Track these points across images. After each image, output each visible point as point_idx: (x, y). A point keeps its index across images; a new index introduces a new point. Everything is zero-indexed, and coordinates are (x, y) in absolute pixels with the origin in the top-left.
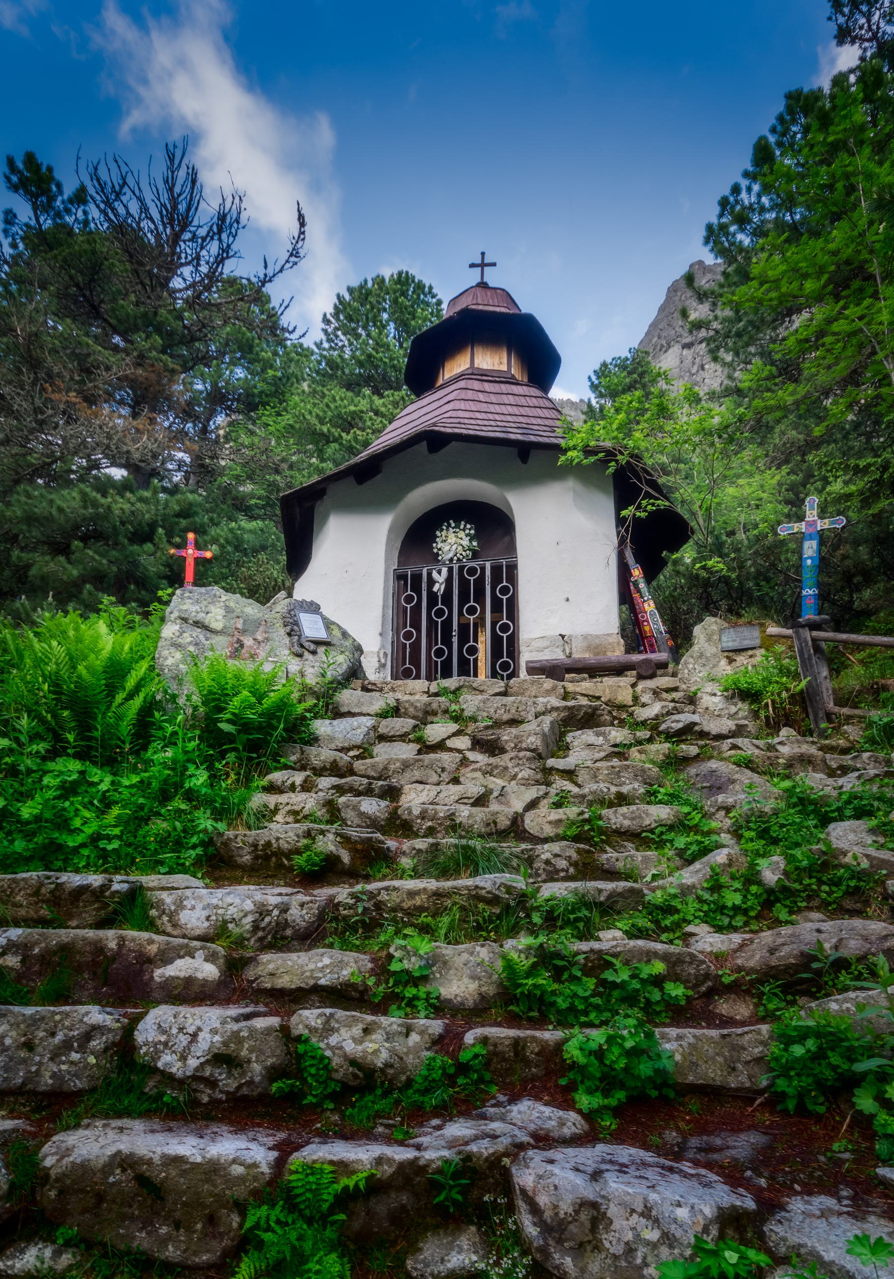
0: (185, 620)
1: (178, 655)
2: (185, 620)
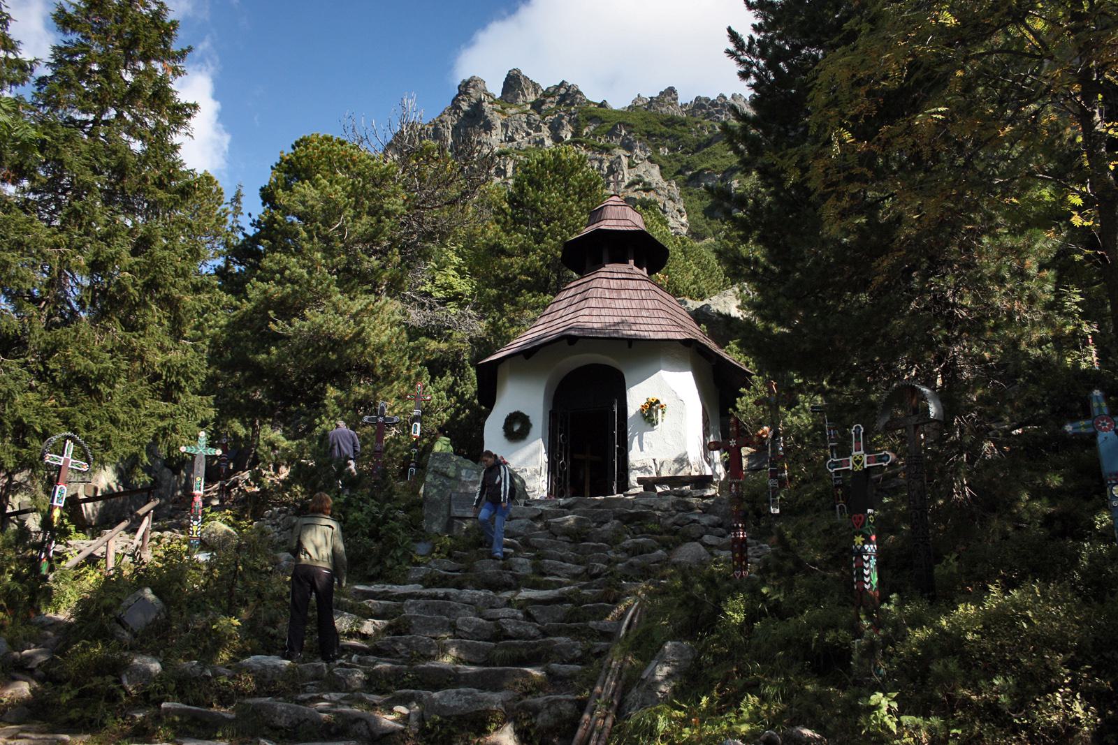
1: (435, 491)
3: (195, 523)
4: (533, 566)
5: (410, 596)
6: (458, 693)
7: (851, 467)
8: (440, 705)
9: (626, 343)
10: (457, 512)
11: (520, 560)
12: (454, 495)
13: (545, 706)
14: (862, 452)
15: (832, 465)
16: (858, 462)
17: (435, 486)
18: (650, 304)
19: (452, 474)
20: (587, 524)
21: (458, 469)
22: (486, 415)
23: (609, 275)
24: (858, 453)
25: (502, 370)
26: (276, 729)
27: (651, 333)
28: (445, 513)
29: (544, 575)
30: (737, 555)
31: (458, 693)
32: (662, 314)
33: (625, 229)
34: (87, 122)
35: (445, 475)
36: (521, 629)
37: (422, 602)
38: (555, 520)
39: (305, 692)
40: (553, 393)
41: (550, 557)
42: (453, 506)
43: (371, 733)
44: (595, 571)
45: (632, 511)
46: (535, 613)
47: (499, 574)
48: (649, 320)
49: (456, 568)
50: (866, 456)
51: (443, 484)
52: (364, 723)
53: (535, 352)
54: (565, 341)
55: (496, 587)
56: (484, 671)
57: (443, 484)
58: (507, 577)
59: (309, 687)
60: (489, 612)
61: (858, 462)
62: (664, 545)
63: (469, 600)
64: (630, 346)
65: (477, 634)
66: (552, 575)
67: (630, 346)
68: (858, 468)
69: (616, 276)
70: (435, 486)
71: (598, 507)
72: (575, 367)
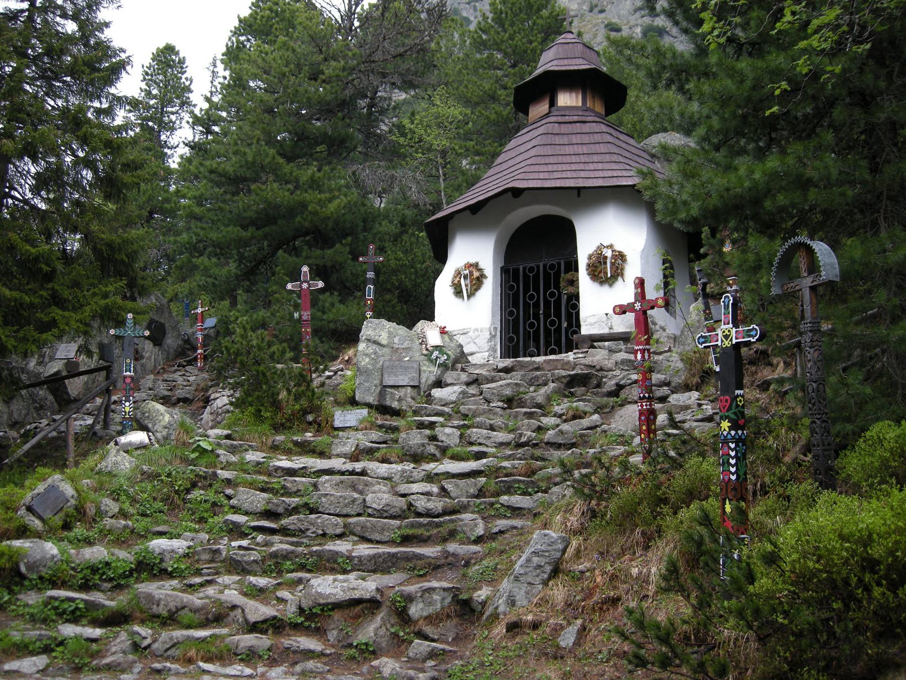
0: (369, 340)
1: (367, 360)
2: (369, 340)
3: (127, 404)
4: (461, 436)
5: (329, 472)
6: (335, 580)
7: (719, 343)
8: (316, 592)
9: (576, 191)
10: (389, 380)
11: (448, 430)
12: (387, 364)
13: (419, 594)
14: (731, 325)
15: (702, 340)
16: (726, 337)
17: (366, 355)
18: (602, 148)
19: (384, 342)
20: (522, 389)
21: (391, 335)
22: (438, 273)
23: (560, 119)
24: (727, 326)
25: (451, 224)
26: (156, 616)
27: (600, 180)
28: (377, 382)
29: (471, 444)
30: (644, 428)
31: (335, 580)
32: (615, 158)
33: (576, 68)
34: (22, 11)
35: (376, 343)
36: (430, 505)
37: (338, 478)
38: (488, 386)
39: (201, 575)
40: (504, 248)
41: (479, 426)
42: (386, 376)
43: (246, 620)
44: (523, 439)
45: (573, 373)
46: (449, 486)
47: (423, 445)
48: (600, 166)
49: (381, 440)
50: (734, 330)
51: (375, 353)
52: (240, 611)
53: (457, 216)
54: (510, 194)
55: (417, 458)
56: (378, 555)
57: (375, 353)
58: (432, 449)
59: (206, 571)
60: (403, 488)
61: (726, 337)
62: (598, 410)
63: (386, 475)
64: (579, 195)
65: (386, 511)
66: (480, 444)
67: (579, 195)
68: (727, 343)
69: (567, 119)
70: (366, 355)
71: (538, 369)
72: (524, 221)
